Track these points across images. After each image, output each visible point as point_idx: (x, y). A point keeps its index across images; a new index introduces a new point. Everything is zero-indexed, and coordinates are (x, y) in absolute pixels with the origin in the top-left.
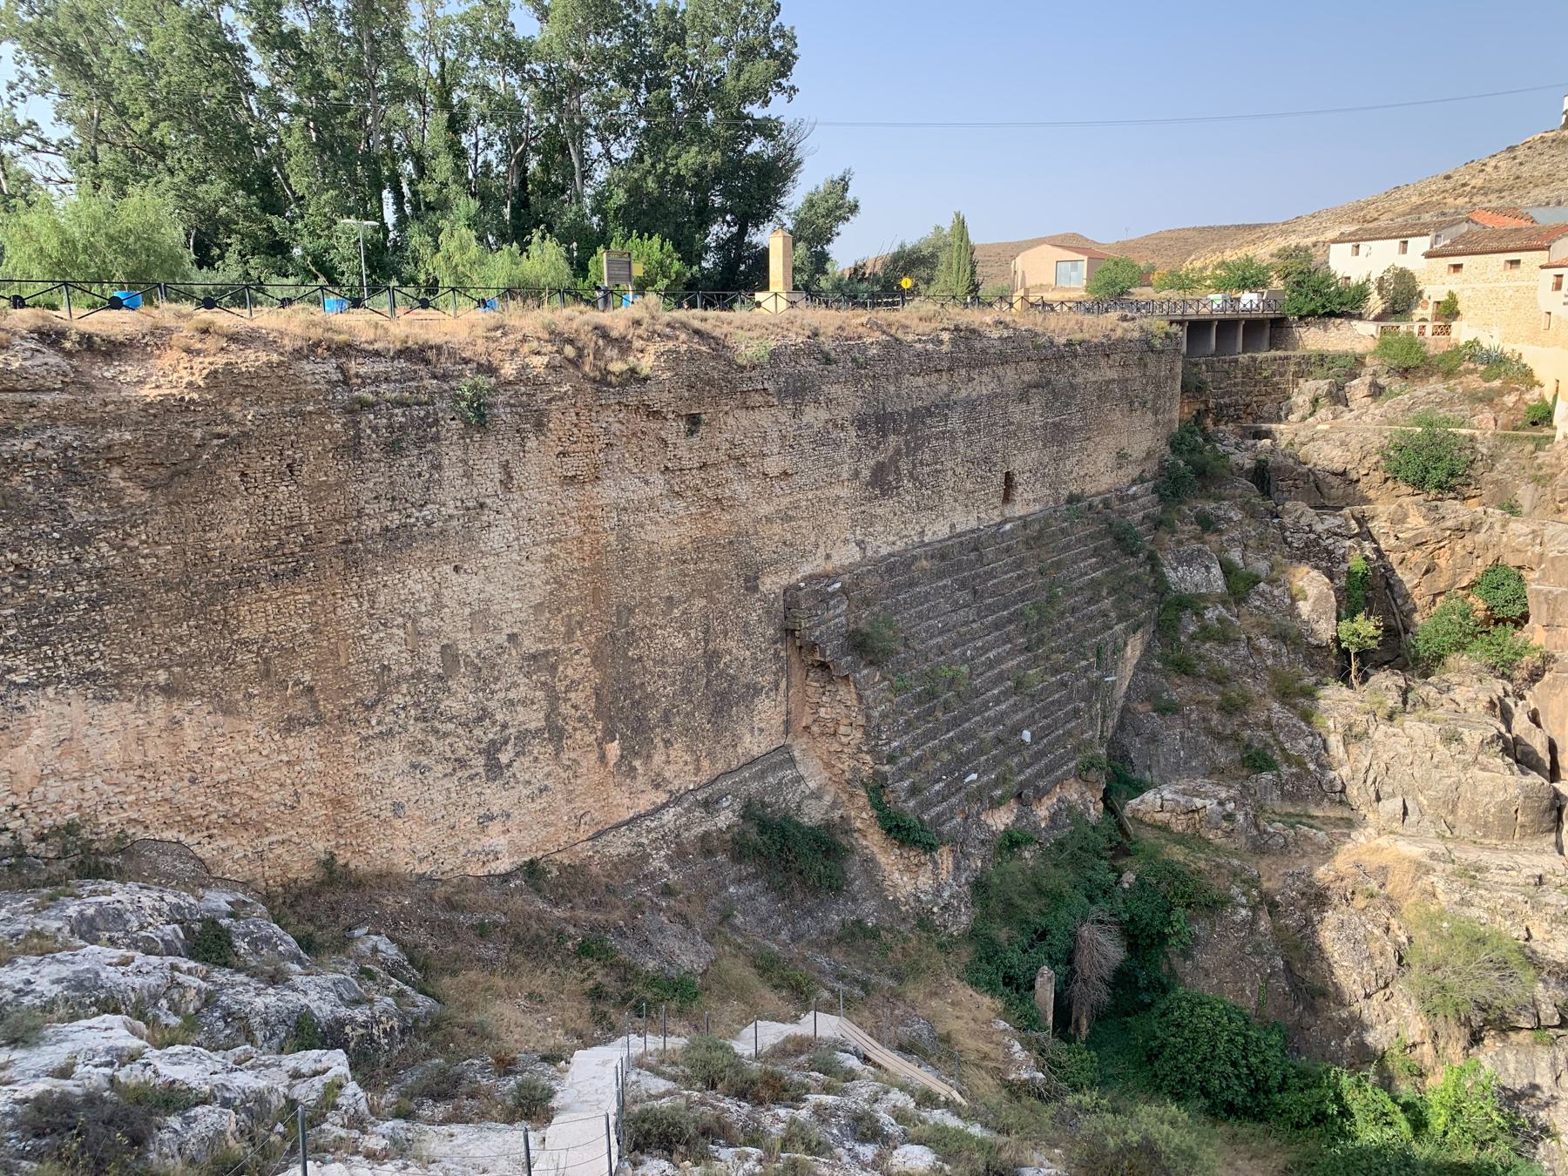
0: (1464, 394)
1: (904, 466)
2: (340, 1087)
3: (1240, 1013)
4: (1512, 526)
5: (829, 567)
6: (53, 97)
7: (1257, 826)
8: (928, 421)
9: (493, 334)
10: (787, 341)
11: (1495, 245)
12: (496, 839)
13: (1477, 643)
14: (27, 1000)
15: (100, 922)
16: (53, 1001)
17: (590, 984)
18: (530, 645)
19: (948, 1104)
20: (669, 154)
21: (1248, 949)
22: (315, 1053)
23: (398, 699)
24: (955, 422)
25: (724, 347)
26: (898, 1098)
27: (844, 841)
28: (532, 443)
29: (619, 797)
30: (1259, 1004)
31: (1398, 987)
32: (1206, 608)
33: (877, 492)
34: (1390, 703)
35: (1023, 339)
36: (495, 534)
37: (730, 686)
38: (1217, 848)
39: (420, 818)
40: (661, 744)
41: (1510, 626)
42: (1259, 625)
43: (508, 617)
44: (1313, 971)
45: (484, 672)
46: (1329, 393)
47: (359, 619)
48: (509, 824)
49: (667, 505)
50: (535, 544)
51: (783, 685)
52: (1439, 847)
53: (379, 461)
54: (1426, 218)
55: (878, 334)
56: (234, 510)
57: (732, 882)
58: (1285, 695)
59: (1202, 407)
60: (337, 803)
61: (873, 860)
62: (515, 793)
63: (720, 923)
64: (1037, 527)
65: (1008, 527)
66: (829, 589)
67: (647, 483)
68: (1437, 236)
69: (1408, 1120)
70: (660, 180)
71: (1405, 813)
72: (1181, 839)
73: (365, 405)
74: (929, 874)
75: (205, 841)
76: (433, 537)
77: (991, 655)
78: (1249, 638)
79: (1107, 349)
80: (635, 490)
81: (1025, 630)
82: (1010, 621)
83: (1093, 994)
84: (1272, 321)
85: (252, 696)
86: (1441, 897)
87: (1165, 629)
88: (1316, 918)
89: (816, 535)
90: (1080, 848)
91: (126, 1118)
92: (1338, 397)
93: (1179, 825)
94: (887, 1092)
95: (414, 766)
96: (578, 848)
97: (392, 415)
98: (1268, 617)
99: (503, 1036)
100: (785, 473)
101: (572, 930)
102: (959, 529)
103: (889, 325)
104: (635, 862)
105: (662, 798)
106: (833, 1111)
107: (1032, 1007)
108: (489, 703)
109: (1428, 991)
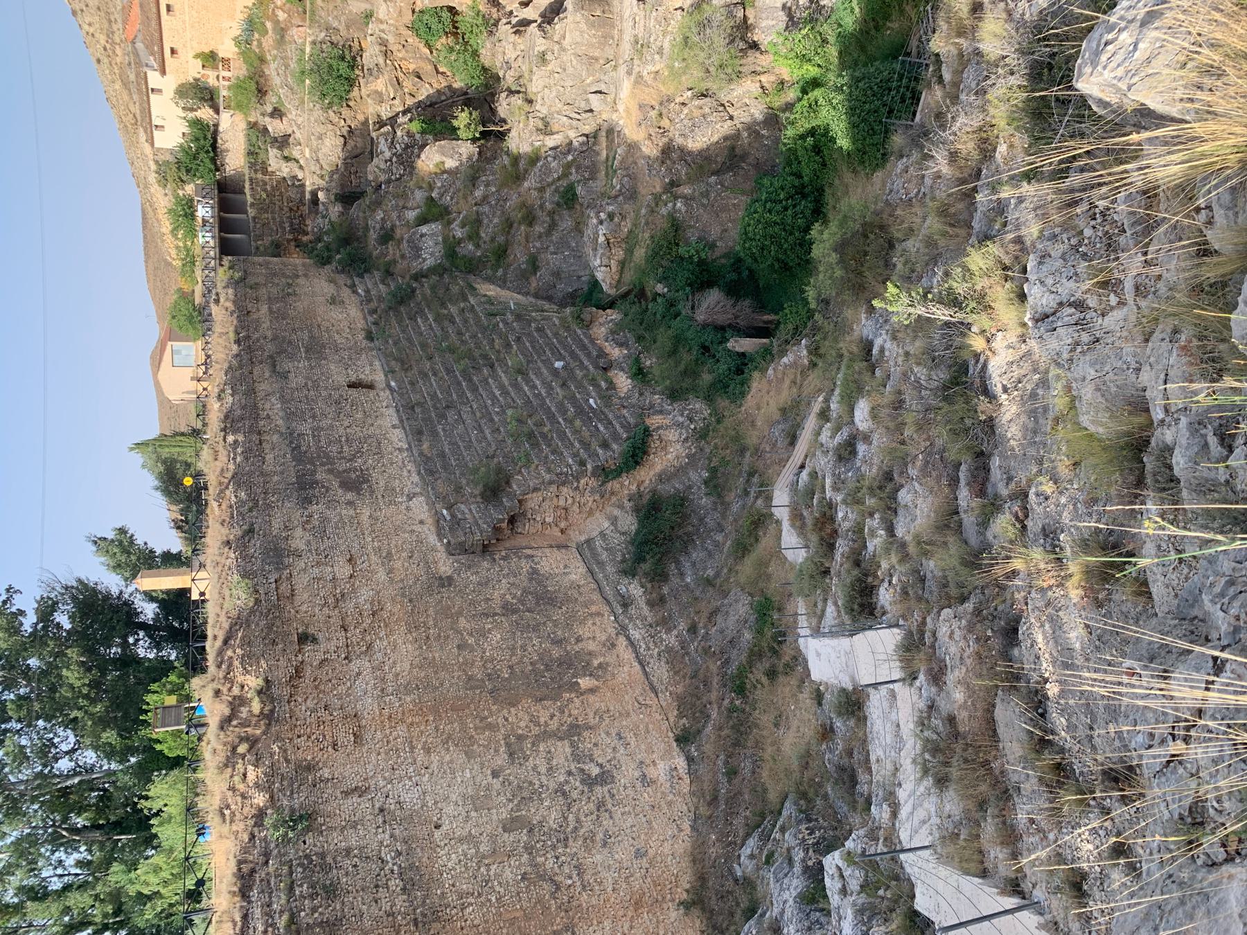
0: (277, 49)
4: (381, 16)
5: (430, 521)
7: (616, 197)
8: (303, 449)
9: (228, 818)
10: (233, 566)
11: (154, 23)
12: (660, 771)
13: (472, 42)
17: (764, 680)
18: (501, 760)
19: (827, 400)
20: (69, 695)
21: (705, 201)
22: (828, 882)
23: (550, 863)
24: (305, 427)
26: (825, 437)
28: (326, 773)
29: (623, 675)
30: (743, 193)
31: (724, 98)
33: (365, 486)
34: (520, 102)
36: (406, 797)
37: (531, 593)
38: (635, 225)
40: (580, 645)
41: (459, 18)
42: (465, 197)
43: (478, 780)
44: (717, 155)
45: (525, 795)
46: (280, 148)
47: (483, 905)
48: (648, 761)
49: (379, 656)
50: (415, 762)
51: (529, 552)
52: (622, 69)
53: (343, 903)
54: (132, 77)
55: (228, 492)
57: (683, 580)
59: (293, 243)
60: (638, 905)
61: (660, 476)
62: (623, 759)
63: (714, 586)
64: (393, 363)
65: (393, 384)
66: (448, 518)
67: (359, 674)
68: (147, 65)
70: (93, 701)
71: (600, 92)
72: (630, 252)
74: (667, 433)
76: (410, 848)
77: (497, 393)
79: (243, 314)
80: (366, 683)
81: (477, 369)
82: (470, 380)
83: (745, 310)
86: (658, 67)
87: (472, 267)
89: (404, 532)
92: (283, 142)
93: (619, 254)
94: (822, 445)
95: (605, 844)
96: (664, 704)
98: (459, 190)
100: (350, 560)
101: (726, 702)
102: (396, 422)
103: (220, 484)
104: (673, 658)
105: (622, 641)
108: (551, 787)
109: (723, 76)
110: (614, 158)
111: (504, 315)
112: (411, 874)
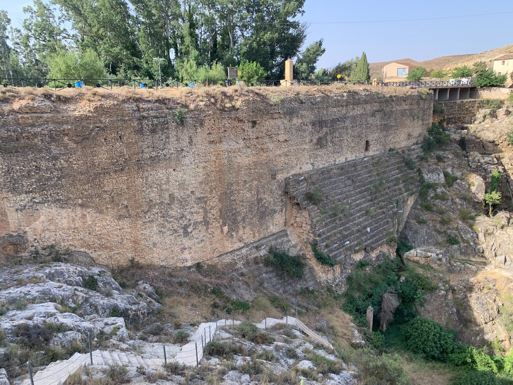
1: (329, 138)
2: (119, 329)
3: (439, 326)
6: (72, 21)
7: (450, 263)
8: (338, 123)
10: (287, 96)
12: (186, 255)
14: (28, 297)
15: (55, 275)
16: (36, 297)
18: (198, 195)
21: (444, 305)
23: (155, 210)
24: (348, 123)
25: (266, 98)
27: (303, 262)
28: (199, 130)
30: (447, 323)
31: (497, 321)
32: (437, 188)
33: (319, 147)
34: (503, 223)
35: (374, 95)
38: (435, 270)
39: (162, 248)
40: (242, 228)
42: (456, 194)
43: (191, 186)
44: (467, 313)
45: (183, 203)
46: (490, 114)
50: (200, 162)
51: (284, 210)
53: (149, 135)
55: (320, 94)
56: (103, 150)
57: (264, 273)
58: (464, 219)
59: (443, 119)
60: (135, 242)
62: (193, 242)
63: (259, 286)
64: (377, 159)
65: (366, 159)
66: (300, 179)
67: (238, 143)
69: (497, 366)
71: (505, 261)
72: (422, 266)
73: (144, 117)
74: (331, 274)
75: (93, 252)
76: (167, 160)
77: (358, 202)
78: (452, 199)
79: (405, 99)
80: (234, 145)
82: (365, 191)
83: (387, 317)
84: (471, 88)
85: (108, 208)
87: (423, 195)
88: (469, 295)
90: (387, 268)
91: (44, 333)
92: (493, 115)
93: (422, 261)
94: (305, 343)
95: (160, 232)
96: (214, 259)
97: (153, 121)
98: (460, 192)
99: (180, 317)
101: (209, 285)
102: (349, 159)
103: (325, 91)
104: (232, 265)
105: (242, 245)
106: (281, 348)
107: (365, 319)
110: (471, 264)
111: (397, 207)
112: (157, 160)
